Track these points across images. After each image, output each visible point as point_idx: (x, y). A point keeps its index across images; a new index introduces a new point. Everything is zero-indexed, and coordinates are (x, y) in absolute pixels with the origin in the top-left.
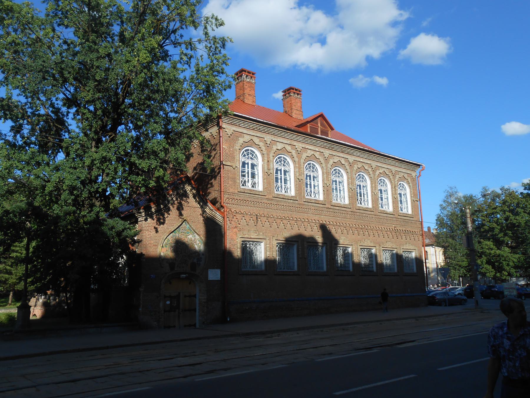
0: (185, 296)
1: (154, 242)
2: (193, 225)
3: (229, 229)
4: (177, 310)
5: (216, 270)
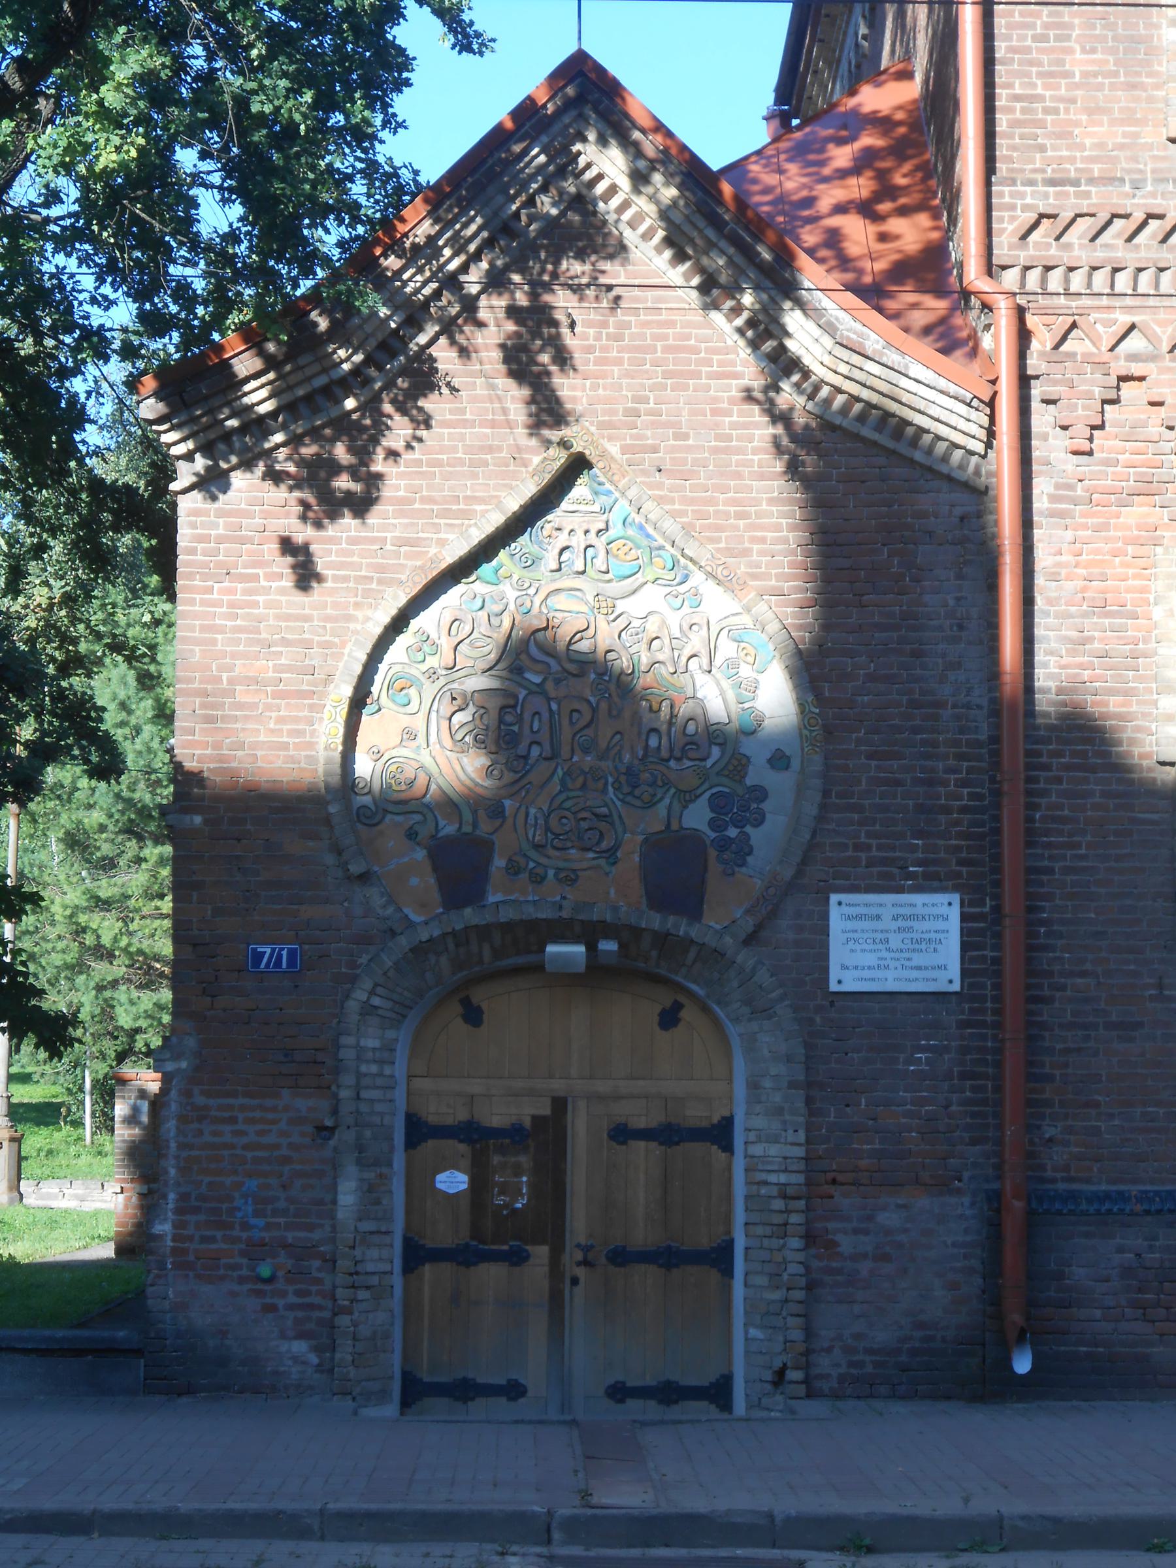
0: (622, 1134)
1: (289, 669)
2: (660, 500)
3: (1062, 514)
4: (541, 1252)
5: (919, 899)
